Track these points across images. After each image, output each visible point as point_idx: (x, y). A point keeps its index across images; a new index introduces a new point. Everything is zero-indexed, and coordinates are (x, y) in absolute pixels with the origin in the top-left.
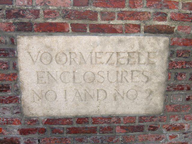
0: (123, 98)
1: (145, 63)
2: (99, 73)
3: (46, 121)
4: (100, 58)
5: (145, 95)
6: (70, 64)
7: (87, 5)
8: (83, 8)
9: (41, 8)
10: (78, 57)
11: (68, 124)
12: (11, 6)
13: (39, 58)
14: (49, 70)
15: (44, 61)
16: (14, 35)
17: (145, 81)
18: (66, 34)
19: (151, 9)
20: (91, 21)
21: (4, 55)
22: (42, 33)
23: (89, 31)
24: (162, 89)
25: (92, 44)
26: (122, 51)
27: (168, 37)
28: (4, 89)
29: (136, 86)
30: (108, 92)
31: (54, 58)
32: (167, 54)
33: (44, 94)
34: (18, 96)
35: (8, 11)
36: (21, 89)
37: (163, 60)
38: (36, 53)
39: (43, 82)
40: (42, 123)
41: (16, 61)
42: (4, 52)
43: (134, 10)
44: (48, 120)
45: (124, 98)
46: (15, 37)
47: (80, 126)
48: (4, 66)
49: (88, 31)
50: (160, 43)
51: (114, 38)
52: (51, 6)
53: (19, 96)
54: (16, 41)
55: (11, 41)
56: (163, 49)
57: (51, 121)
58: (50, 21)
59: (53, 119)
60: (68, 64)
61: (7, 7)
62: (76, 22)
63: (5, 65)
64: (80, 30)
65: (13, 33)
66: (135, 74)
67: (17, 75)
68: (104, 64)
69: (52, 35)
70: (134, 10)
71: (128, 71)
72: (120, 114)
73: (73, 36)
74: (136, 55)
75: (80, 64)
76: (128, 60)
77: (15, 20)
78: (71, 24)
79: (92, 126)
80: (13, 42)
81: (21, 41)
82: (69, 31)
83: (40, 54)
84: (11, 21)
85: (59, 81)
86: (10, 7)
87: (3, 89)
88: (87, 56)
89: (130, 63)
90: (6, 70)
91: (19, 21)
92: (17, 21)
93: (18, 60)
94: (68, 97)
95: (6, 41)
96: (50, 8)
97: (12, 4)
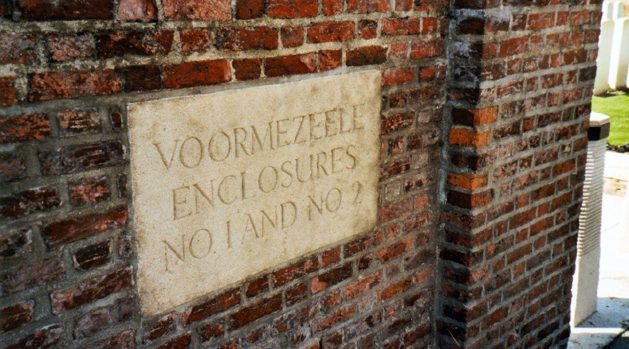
0: (320, 211)
1: (349, 131)
2: (285, 166)
3: (191, 315)
4: (284, 132)
5: (352, 196)
6: (237, 156)
7: (260, 16)
8: (253, 21)
9: (175, 26)
10: (250, 138)
11: (232, 304)
12: (109, 24)
13: (177, 154)
14: (198, 180)
15: (188, 160)
16: (119, 103)
17: (351, 167)
18: (225, 87)
19: (354, 14)
20: (268, 52)
21: (96, 163)
22: (180, 90)
23: (264, 75)
24: (374, 176)
25: (271, 104)
26: (318, 110)
27: (379, 69)
28: (95, 258)
29: (339, 180)
30: (298, 205)
31: (206, 150)
32: (379, 105)
33: (187, 243)
34: (127, 269)
35: (102, 36)
36: (137, 246)
37: (374, 117)
38: (171, 143)
39: (186, 213)
40: (180, 322)
41: (125, 173)
42: (96, 153)
43: (331, 19)
44: (195, 309)
45: (323, 212)
46: (123, 107)
47: (254, 300)
48: (96, 191)
49: (263, 75)
50: (364, 84)
51: (301, 83)
52: (196, 20)
53: (131, 267)
54: (125, 118)
55: (114, 120)
56: (373, 95)
57: (200, 310)
58: (194, 57)
59: (205, 304)
60: (232, 155)
61: (99, 25)
62: (242, 55)
63: (99, 188)
64: (251, 75)
65: (116, 98)
66: (338, 154)
67: (126, 209)
68: (291, 145)
69: (200, 92)
70: (331, 19)
71: (326, 152)
72: (319, 248)
73: (239, 90)
74: (337, 114)
75: (253, 153)
76: (327, 128)
77: (118, 61)
78: (234, 63)
79: (274, 292)
80: (119, 121)
81: (138, 117)
82: (230, 80)
83: (179, 144)
84: (110, 65)
85: (217, 201)
86: (106, 25)
87: (92, 257)
88: (264, 132)
89: (329, 133)
90: (103, 203)
91: (128, 64)
92: (124, 63)
93: (132, 169)
94: (233, 238)
95: (100, 120)
96: (194, 24)
97: (111, 17)
